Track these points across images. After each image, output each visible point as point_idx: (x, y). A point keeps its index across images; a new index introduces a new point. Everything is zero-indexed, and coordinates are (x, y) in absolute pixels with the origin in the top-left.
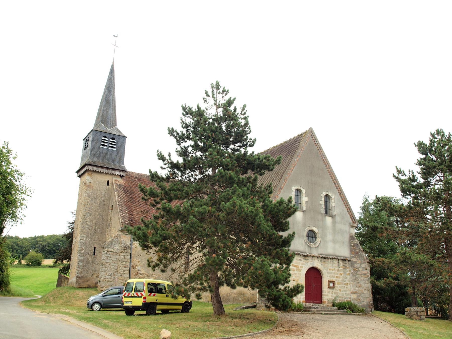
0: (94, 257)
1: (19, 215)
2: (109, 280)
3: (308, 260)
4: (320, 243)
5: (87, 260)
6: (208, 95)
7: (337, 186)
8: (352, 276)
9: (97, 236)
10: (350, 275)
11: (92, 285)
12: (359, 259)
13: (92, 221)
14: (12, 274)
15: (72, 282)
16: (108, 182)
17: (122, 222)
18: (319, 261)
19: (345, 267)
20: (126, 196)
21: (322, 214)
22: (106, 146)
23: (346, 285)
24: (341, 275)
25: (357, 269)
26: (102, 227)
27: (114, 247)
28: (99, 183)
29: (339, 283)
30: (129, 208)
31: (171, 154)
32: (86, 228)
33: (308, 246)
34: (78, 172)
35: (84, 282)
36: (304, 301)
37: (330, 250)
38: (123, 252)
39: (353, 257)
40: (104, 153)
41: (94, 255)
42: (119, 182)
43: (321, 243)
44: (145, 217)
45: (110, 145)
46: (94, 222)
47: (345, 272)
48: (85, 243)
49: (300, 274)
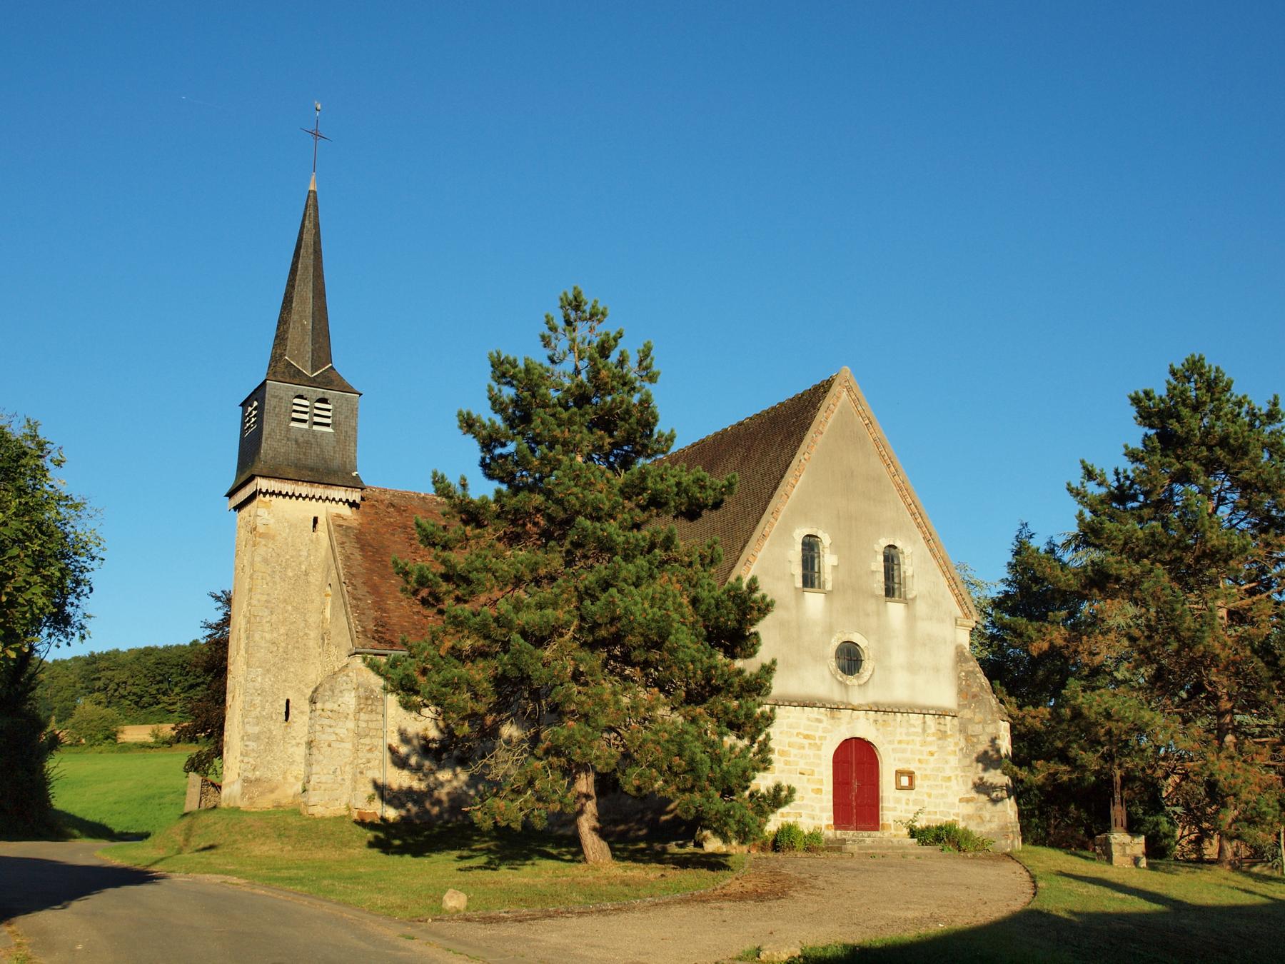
0: (287, 726)
1: (76, 614)
3: (839, 719)
4: (871, 675)
5: (268, 735)
6: (553, 329)
7: (919, 520)
8: (961, 756)
9: (292, 670)
10: (956, 755)
12: (980, 712)
14: (57, 777)
15: (230, 794)
16: (315, 520)
18: (871, 720)
19: (943, 735)
20: (365, 557)
21: (877, 597)
22: (304, 421)
24: (932, 754)
25: (975, 740)
26: (305, 645)
28: (291, 526)
29: (926, 777)
30: (374, 590)
32: (262, 648)
34: (231, 494)
35: (262, 794)
37: (899, 692)
39: (964, 706)
41: (287, 719)
43: (875, 673)
45: (317, 419)
46: (282, 631)
47: (941, 748)
48: (263, 690)
49: (819, 757)
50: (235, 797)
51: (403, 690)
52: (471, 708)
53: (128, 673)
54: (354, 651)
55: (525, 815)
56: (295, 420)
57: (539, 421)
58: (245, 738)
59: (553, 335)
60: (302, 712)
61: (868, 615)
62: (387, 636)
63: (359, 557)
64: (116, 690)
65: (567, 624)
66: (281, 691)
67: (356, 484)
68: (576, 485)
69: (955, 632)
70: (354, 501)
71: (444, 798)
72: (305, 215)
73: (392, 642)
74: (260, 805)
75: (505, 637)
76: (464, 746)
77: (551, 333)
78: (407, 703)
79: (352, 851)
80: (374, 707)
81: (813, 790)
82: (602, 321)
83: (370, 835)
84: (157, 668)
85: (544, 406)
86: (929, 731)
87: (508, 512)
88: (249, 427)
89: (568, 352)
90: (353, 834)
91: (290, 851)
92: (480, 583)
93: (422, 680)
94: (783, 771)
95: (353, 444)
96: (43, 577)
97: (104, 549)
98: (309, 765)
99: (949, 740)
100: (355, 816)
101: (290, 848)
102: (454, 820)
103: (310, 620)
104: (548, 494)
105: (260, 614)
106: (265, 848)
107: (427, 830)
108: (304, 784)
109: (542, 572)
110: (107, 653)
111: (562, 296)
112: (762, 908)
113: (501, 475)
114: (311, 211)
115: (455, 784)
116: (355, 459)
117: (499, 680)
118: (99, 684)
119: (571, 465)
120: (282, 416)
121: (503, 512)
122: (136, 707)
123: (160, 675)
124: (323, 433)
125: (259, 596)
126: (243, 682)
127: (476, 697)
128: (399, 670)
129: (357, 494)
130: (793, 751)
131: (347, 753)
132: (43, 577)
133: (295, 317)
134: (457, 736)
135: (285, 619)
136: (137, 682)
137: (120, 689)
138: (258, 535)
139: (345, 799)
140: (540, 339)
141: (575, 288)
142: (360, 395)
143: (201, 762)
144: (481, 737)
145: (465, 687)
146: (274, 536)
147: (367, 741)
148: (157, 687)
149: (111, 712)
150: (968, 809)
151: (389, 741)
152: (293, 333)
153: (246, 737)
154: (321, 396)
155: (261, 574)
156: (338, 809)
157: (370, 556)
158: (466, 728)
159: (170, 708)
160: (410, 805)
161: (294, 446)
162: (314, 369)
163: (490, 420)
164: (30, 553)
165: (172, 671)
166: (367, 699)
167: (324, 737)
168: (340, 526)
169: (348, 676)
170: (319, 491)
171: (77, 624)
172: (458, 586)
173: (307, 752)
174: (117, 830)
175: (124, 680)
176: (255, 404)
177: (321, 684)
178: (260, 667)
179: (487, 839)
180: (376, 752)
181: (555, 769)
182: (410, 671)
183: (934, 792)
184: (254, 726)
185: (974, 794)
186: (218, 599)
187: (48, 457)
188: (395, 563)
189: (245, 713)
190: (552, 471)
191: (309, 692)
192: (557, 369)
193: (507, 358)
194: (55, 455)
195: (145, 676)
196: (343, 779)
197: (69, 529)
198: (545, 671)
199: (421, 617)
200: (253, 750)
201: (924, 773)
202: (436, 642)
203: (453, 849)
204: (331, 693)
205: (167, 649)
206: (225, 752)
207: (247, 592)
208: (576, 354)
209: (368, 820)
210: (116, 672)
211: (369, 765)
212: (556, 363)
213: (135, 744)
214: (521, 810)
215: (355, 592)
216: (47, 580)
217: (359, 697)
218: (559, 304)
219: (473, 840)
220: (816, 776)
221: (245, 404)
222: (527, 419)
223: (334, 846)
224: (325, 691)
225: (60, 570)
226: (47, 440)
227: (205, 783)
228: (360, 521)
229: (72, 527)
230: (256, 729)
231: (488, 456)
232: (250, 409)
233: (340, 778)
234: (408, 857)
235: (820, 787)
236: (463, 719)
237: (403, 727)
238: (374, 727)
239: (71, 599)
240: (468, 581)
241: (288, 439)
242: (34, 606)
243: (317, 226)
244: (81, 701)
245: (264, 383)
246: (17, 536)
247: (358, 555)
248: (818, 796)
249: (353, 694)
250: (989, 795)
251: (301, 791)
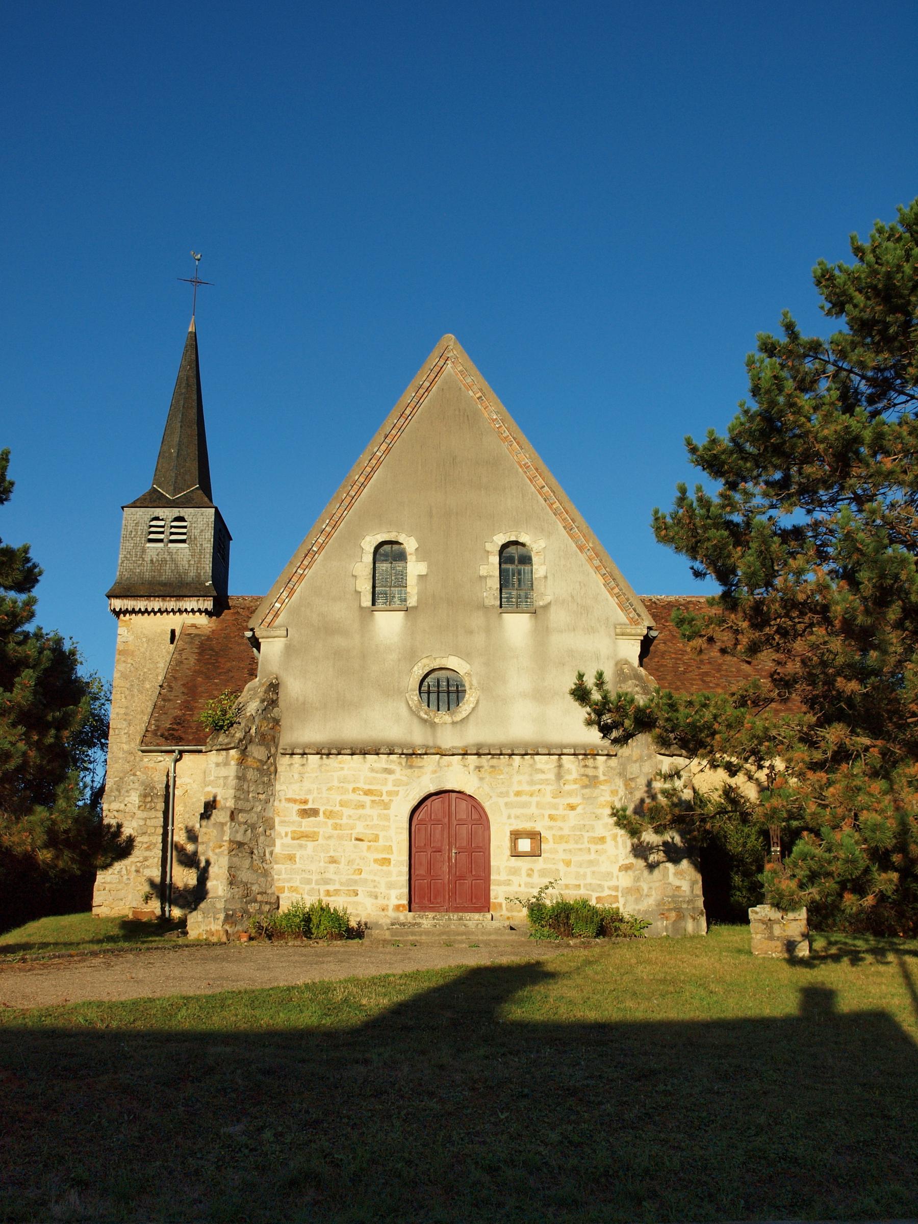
2: (114, 886)
3: (420, 767)
4: (474, 709)
18: (472, 767)
19: (592, 782)
22: (161, 541)
23: (596, 844)
24: (572, 808)
27: (127, 799)
28: (148, 641)
29: (561, 839)
32: (120, 758)
33: (425, 721)
36: (403, 906)
40: (154, 559)
43: (480, 705)
49: (387, 818)
56: (150, 541)
61: (471, 632)
69: (614, 643)
81: (376, 861)
86: (568, 777)
94: (330, 837)
99: (602, 787)
105: (119, 727)
125: (117, 710)
129: (209, 602)
130: (346, 811)
146: (133, 652)
150: (625, 880)
154: (177, 515)
157: (207, 659)
170: (171, 604)
183: (575, 859)
185: (632, 860)
201: (560, 833)
204: (117, 793)
220: (381, 842)
235: (387, 856)
238: (152, 825)
248: (384, 868)
250: (646, 859)
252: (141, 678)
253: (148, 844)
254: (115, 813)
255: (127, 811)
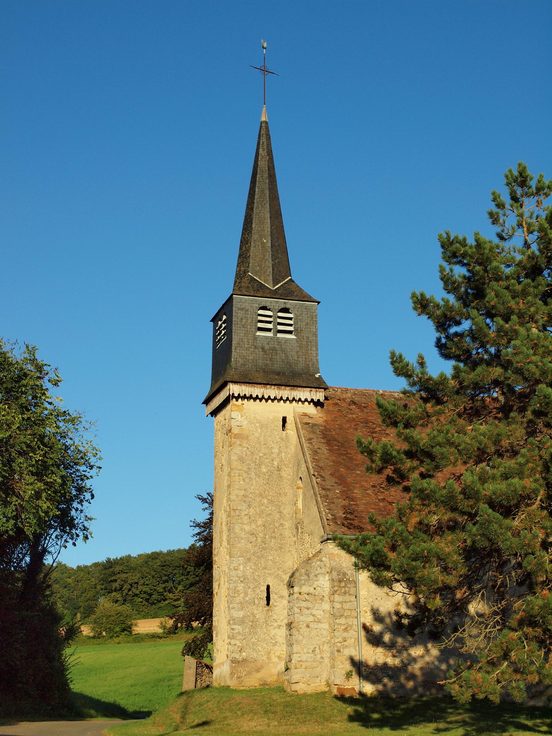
0: (268, 610)
5: (252, 619)
6: (500, 206)
9: (270, 558)
11: (269, 680)
13: (255, 521)
14: (73, 664)
16: (284, 420)
17: (327, 520)
22: (269, 330)
26: (281, 534)
27: (316, 583)
28: (262, 426)
30: (341, 481)
31: (426, 359)
34: (207, 402)
35: (249, 673)
38: (338, 592)
41: (268, 604)
42: (312, 418)
44: (384, 500)
45: (280, 328)
46: (260, 522)
50: (225, 677)
51: (374, 566)
52: (442, 581)
53: (139, 575)
54: (325, 538)
55: (502, 687)
56: (261, 329)
57: (493, 294)
58: (231, 622)
59: (501, 212)
60: (282, 597)
62: (356, 523)
63: (326, 451)
64: (129, 590)
65: (535, 492)
66: (261, 578)
67: (320, 385)
68: (535, 354)
70: (319, 400)
71: (418, 673)
72: (258, 144)
73: (361, 528)
74: (248, 684)
75: (472, 509)
76: (436, 620)
77: (498, 210)
78: (378, 578)
79: (333, 725)
80: (347, 589)
82: (549, 195)
83: (350, 709)
84: (163, 569)
85: (498, 279)
87: (468, 387)
88: (220, 339)
89: (517, 227)
90: (333, 709)
91: (275, 726)
92: (443, 457)
93: (392, 556)
95: (314, 349)
96: (46, 483)
97: (100, 459)
98: (291, 645)
100: (335, 691)
101: (276, 723)
102: (428, 693)
103: (285, 512)
104: (506, 365)
105: (239, 508)
106: (253, 724)
107: (403, 704)
108: (286, 663)
109: (505, 443)
110: (121, 558)
111: (508, 173)
112: (99, 646)
113: (457, 353)
114: (263, 139)
115: (427, 659)
116: (317, 362)
117: (469, 552)
118: (116, 585)
119: (528, 335)
120: (249, 327)
121: (462, 388)
122: (147, 603)
123: (166, 575)
124: (287, 340)
125: (236, 492)
126: (227, 571)
127: (445, 570)
128: (369, 547)
129: (321, 394)
131: (325, 633)
132: (46, 483)
133: (255, 236)
134: (429, 610)
135: (262, 512)
136: (147, 582)
137: (133, 589)
138: (233, 436)
139: (325, 676)
140: (487, 216)
141: (520, 165)
142: (319, 303)
143: (197, 647)
144: (452, 611)
145: (435, 561)
147: (342, 621)
148: (164, 586)
149: (126, 608)
151: (363, 620)
152: (254, 251)
153: (232, 621)
154: (282, 306)
155: (237, 472)
156: (319, 685)
158: (438, 602)
159: (175, 603)
160: (386, 680)
161: (261, 353)
162: (275, 282)
163: (443, 300)
164: (34, 462)
165: (175, 571)
166: (340, 581)
167: (302, 618)
168: (307, 424)
169: (321, 561)
170: (286, 393)
171: (80, 526)
172: (422, 462)
173: (288, 633)
174: (131, 709)
175: (136, 581)
176: (224, 317)
177: (297, 570)
178: (242, 556)
179: (461, 711)
180: (351, 632)
181: (532, 640)
182: (380, 546)
184: (239, 610)
186: (204, 500)
187: (47, 378)
188: (359, 443)
189: (230, 599)
190: (509, 342)
191: (286, 578)
192: (506, 245)
193: (456, 238)
194: (52, 375)
195: (153, 577)
196: (322, 658)
197: (69, 442)
198: (515, 540)
199: (386, 504)
200: (239, 633)
202: (404, 519)
203: (430, 721)
204: (306, 577)
205: (170, 553)
206: (214, 635)
207: (226, 488)
208: (525, 229)
209: (347, 695)
210: (129, 574)
211: (345, 643)
212: (505, 240)
213: (147, 635)
214: (498, 682)
215: (324, 483)
216: (51, 487)
217: (333, 580)
218: (505, 181)
219: (447, 712)
221: (215, 320)
222: (480, 294)
223: (317, 721)
224: (301, 575)
225: (62, 477)
226: (44, 363)
227: (199, 665)
228: (325, 418)
229: (71, 439)
230: (241, 614)
231: (443, 336)
232: (220, 323)
233: (319, 656)
234: (386, 730)
236: (435, 592)
237: (375, 607)
238: (348, 608)
239: (75, 505)
240: (430, 456)
241: (255, 347)
242: (40, 509)
243: (270, 153)
244: (101, 600)
245: (231, 298)
246: (22, 449)
247: (324, 449)
249: (327, 577)
251: (284, 669)
252: (258, 461)
253: (346, 626)
254: (306, 596)
255: (317, 594)
